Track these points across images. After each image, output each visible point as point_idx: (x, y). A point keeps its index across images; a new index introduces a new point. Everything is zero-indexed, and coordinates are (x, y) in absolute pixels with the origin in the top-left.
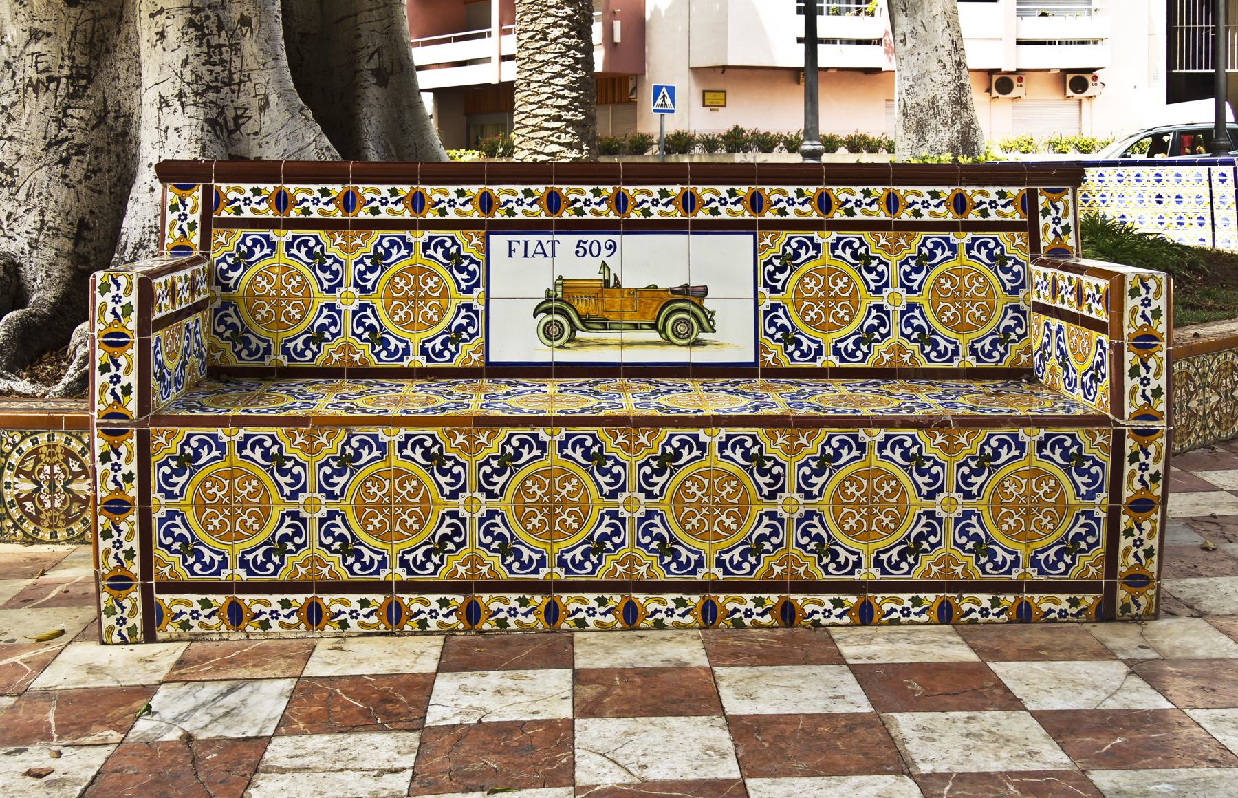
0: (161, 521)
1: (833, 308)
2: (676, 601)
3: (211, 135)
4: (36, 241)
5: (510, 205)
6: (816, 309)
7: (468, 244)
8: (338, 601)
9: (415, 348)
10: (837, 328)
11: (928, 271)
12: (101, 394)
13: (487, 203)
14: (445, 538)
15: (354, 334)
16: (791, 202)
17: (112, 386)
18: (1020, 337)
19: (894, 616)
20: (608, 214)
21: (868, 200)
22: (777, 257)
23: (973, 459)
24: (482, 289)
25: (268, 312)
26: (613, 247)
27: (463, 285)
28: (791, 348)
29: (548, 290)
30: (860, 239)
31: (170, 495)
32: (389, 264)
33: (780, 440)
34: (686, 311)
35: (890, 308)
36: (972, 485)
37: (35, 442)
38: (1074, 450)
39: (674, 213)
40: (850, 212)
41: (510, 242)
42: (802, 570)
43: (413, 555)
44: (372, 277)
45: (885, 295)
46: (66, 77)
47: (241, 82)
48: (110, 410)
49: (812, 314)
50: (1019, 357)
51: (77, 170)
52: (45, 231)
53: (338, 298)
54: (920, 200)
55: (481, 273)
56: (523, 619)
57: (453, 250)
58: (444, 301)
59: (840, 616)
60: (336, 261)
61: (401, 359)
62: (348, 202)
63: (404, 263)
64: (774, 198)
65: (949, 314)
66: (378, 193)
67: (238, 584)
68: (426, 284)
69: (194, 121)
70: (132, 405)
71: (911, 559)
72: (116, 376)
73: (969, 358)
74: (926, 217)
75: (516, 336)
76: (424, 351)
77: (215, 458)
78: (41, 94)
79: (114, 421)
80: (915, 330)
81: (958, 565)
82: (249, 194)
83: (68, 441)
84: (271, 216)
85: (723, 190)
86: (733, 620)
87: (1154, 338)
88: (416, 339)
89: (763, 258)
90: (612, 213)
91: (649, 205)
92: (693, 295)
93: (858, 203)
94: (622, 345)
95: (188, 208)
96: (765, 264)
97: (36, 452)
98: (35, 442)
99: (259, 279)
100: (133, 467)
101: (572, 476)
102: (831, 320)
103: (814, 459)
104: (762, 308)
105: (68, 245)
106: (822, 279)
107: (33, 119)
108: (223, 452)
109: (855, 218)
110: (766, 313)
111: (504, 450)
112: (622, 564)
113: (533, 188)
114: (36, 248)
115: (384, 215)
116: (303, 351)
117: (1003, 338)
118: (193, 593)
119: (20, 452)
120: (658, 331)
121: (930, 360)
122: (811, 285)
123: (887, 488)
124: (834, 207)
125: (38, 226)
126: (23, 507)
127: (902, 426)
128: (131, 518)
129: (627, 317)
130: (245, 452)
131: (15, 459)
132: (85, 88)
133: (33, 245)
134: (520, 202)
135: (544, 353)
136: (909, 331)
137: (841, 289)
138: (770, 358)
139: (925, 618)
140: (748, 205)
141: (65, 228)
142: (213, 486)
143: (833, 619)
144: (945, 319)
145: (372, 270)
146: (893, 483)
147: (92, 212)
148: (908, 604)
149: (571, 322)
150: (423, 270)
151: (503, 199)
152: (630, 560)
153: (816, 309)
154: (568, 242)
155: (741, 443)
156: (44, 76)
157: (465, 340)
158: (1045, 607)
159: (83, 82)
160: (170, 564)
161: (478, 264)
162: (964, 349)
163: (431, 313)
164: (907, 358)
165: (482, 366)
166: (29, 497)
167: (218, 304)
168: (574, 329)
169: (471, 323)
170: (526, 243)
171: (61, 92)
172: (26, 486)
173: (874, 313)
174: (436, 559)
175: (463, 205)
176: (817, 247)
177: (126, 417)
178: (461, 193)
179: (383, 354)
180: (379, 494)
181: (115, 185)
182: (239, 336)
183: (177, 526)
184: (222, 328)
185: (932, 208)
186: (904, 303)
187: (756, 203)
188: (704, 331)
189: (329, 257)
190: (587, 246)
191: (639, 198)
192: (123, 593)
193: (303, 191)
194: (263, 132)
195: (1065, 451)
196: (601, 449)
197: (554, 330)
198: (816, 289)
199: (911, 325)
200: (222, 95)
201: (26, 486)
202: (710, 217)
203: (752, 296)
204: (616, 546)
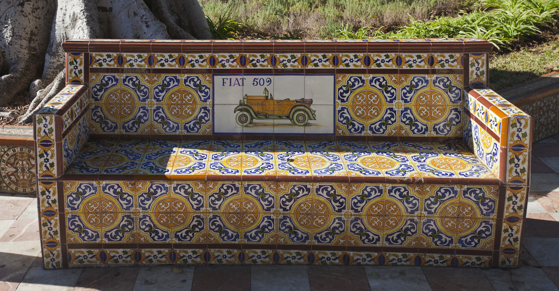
0: (69, 219)
1: (370, 109)
2: (296, 253)
5: (223, 62)
6: (362, 110)
7: (205, 80)
8: (148, 251)
12: (40, 167)
13: (213, 61)
14: (194, 226)
16: (351, 61)
17: (45, 163)
19: (394, 262)
20: (267, 66)
21: (387, 60)
22: (344, 86)
23: (432, 197)
24: (211, 100)
25: (116, 110)
26: (270, 81)
27: (203, 98)
28: (350, 127)
29: (241, 101)
30: (383, 78)
31: (73, 209)
32: (169, 89)
33: (344, 188)
35: (396, 109)
36: (432, 208)
37: (14, 151)
38: (481, 195)
39: (298, 66)
40: (379, 65)
41: (223, 79)
45: (394, 103)
48: (45, 174)
49: (360, 112)
54: (412, 59)
55: (210, 93)
57: (198, 82)
59: (370, 261)
63: (176, 88)
64: (344, 59)
65: (424, 112)
67: (104, 244)
68: (186, 98)
71: (402, 238)
72: (47, 159)
73: (433, 132)
74: (415, 68)
75: (227, 120)
77: (93, 193)
79: (46, 178)
82: (105, 57)
84: (116, 67)
85: (320, 55)
86: (322, 262)
89: (338, 87)
90: (269, 66)
91: (286, 62)
92: (306, 103)
93: (383, 61)
94: (274, 125)
95: (78, 63)
96: (339, 89)
97: (15, 155)
98: (14, 151)
99: (111, 95)
100: (56, 197)
102: (369, 115)
103: (359, 196)
106: (365, 96)
108: (96, 191)
109: (381, 68)
110: (339, 111)
111: (220, 190)
112: (272, 237)
113: (234, 54)
115: (167, 67)
116: (132, 127)
118: (84, 248)
119: (8, 155)
120: (290, 119)
121: (414, 133)
122: (360, 98)
123: (392, 209)
124: (371, 63)
126: (10, 178)
127: (399, 183)
128: (56, 218)
129: (276, 113)
130: (106, 191)
131: (5, 158)
134: (228, 61)
135: (239, 129)
136: (405, 120)
137: (374, 101)
138: (340, 131)
139: (408, 263)
140: (332, 62)
142: (92, 205)
143: (366, 262)
144: (422, 115)
145: (162, 91)
146: (395, 207)
147: (36, 27)
148: (401, 257)
149: (251, 115)
150: (184, 91)
151: (220, 59)
152: (276, 237)
153: (362, 110)
154: (249, 79)
155: (326, 189)
161: (209, 89)
163: (188, 111)
164: (403, 132)
165: (211, 134)
166: (13, 174)
168: (252, 118)
169: (206, 115)
170: (231, 79)
172: (11, 170)
173: (389, 112)
174: (191, 235)
175: (202, 62)
176: (363, 81)
177: (52, 176)
178: (201, 57)
180: (165, 208)
181: (46, 15)
182: (103, 121)
183: (76, 221)
184: (96, 117)
185: (417, 63)
186: (403, 107)
187: (335, 61)
188: (311, 119)
189: (142, 86)
190: (258, 81)
191: (281, 59)
192: (53, 248)
195: (476, 195)
196: (263, 191)
198: (362, 100)
199: (406, 117)
201: (11, 170)
202: (314, 68)
203: (333, 104)
204: (270, 230)
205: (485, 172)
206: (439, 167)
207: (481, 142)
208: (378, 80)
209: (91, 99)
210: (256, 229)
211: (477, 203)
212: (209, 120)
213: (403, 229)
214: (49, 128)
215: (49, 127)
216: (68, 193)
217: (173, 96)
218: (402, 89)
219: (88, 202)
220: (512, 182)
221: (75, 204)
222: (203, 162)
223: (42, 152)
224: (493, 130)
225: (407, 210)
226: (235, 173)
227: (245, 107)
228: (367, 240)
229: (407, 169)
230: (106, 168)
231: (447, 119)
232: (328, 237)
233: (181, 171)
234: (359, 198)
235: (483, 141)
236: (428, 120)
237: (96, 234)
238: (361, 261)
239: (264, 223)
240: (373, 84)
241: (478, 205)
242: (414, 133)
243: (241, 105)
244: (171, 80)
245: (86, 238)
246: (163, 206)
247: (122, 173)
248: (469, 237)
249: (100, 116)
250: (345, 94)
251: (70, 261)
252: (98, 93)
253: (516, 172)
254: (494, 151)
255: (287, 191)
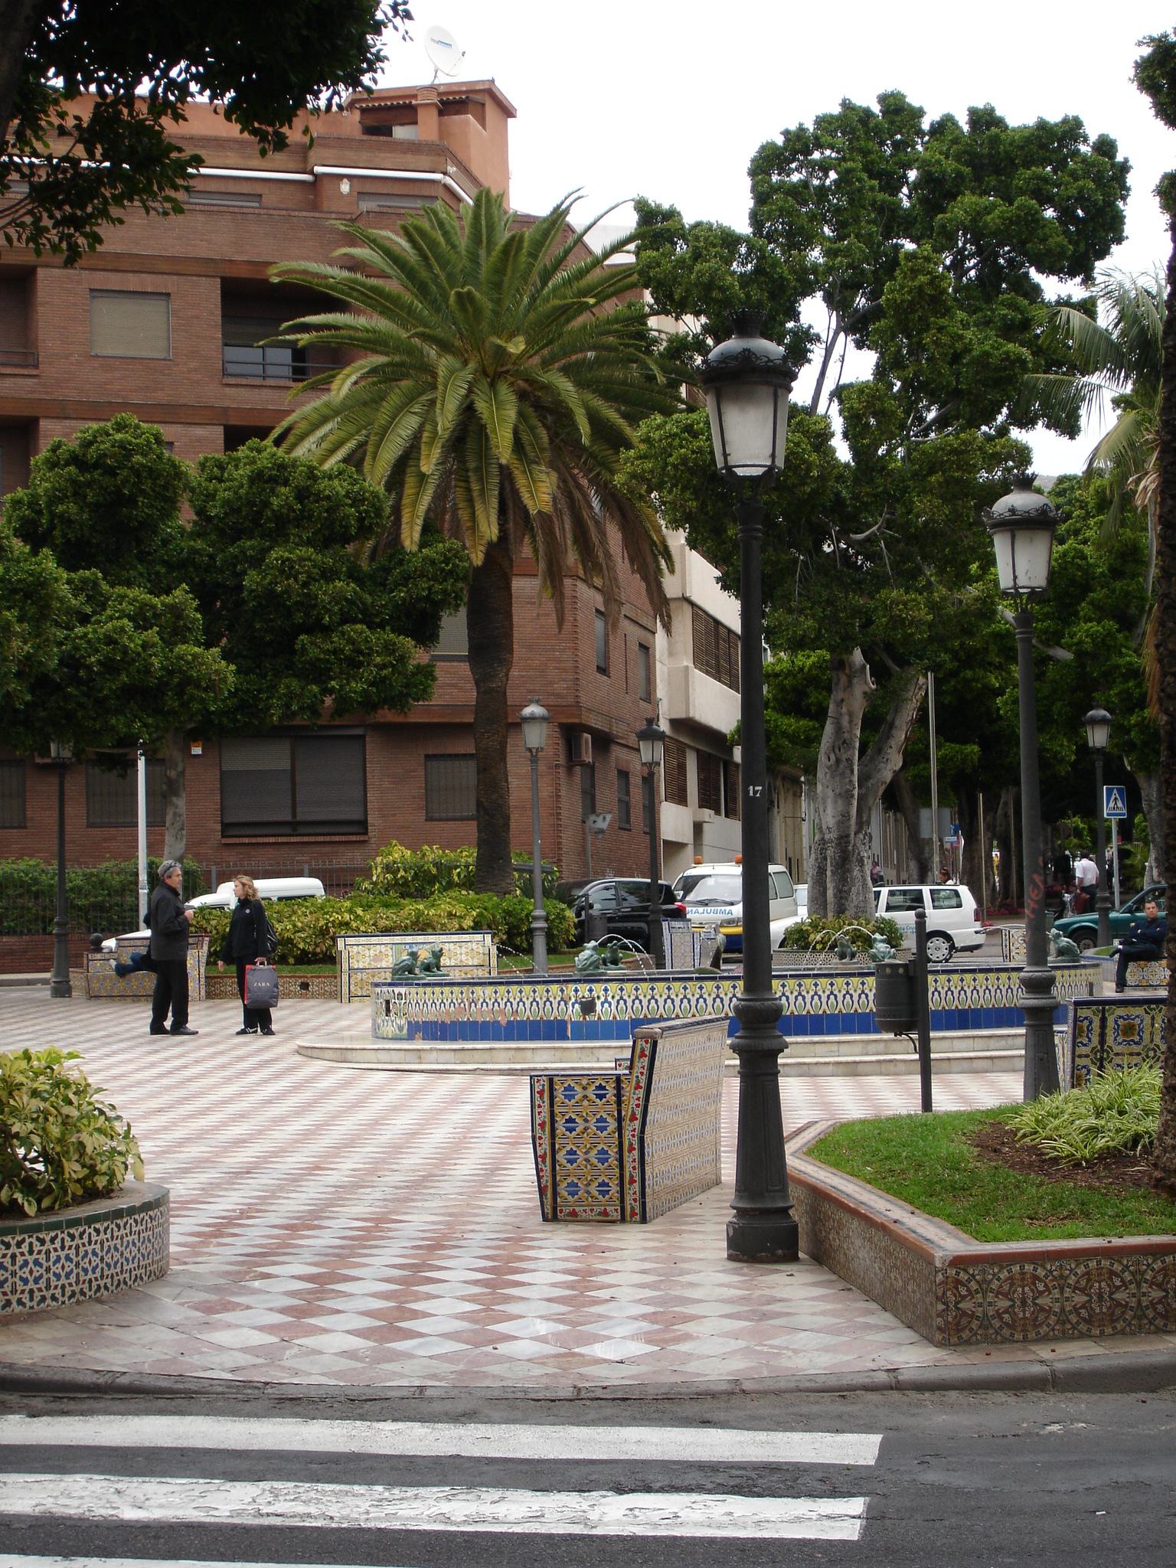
37: (1163, 1262)
83: (1035, 1269)
97: (1011, 1278)
119: (1076, 1274)
126: (1079, 1314)
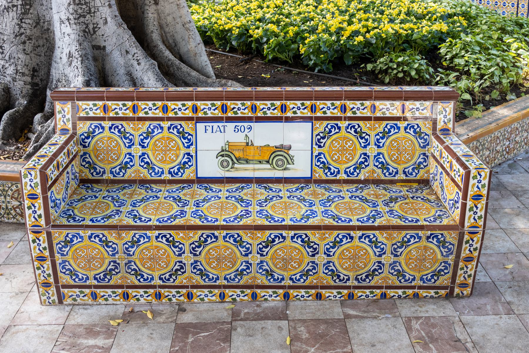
0: (60, 264)
3: (83, 38)
4: (15, 78)
5: (205, 110)
7: (188, 127)
9: (166, 171)
10: (347, 163)
11: (387, 138)
12: (29, 218)
13: (195, 109)
14: (177, 270)
15: (140, 165)
16: (329, 108)
17: (33, 215)
18: (425, 166)
26: (250, 128)
30: (358, 124)
32: (154, 136)
33: (317, 235)
34: (282, 155)
35: (370, 154)
37: (17, 187)
38: (442, 239)
41: (206, 126)
42: (325, 281)
43: (164, 276)
44: (147, 141)
45: (368, 148)
46: (21, 5)
47: (95, 12)
49: (336, 157)
50: (424, 175)
51: (29, 47)
52: (18, 74)
53: (133, 150)
56: (211, 298)
58: (178, 152)
60: (131, 135)
61: (160, 176)
62: (134, 109)
63: (160, 136)
65: (395, 157)
66: (148, 105)
69: (75, 32)
70: (42, 222)
73: (402, 175)
75: (209, 166)
76: (170, 173)
77: (80, 242)
78: (10, 13)
80: (380, 163)
81: (390, 280)
87: (482, 196)
88: (166, 168)
89: (315, 133)
91: (266, 110)
93: (358, 109)
94: (254, 170)
96: (317, 136)
98: (17, 187)
99: (98, 142)
100: (46, 245)
101: (229, 248)
104: (314, 154)
105: (29, 79)
106: (341, 142)
107: (8, 24)
110: (316, 156)
114: (16, 81)
116: (119, 173)
117: (418, 167)
123: (362, 253)
124: (347, 110)
125: (15, 71)
126: (16, 211)
132: (29, 9)
133: (14, 80)
134: (210, 109)
137: (349, 146)
141: (27, 72)
144: (393, 159)
147: (38, 64)
149: (232, 160)
150: (168, 138)
154: (231, 126)
156: (10, 5)
157: (187, 168)
158: (425, 295)
159: (28, 7)
160: (65, 279)
161: (192, 135)
162: (401, 172)
163: (172, 157)
165: (195, 178)
166: (17, 207)
167: (82, 153)
168: (234, 163)
169: (190, 161)
170: (212, 126)
171: (19, 12)
177: (41, 227)
178: (184, 105)
179: (153, 174)
181: (46, 52)
182: (92, 166)
186: (376, 152)
187: (313, 109)
190: (239, 128)
193: (115, 104)
194: (106, 35)
197: (225, 164)
199: (378, 161)
200: (87, 18)
205: (447, 217)
206: (406, 213)
207: (445, 187)
208: (331, 174)
209: (79, 146)
210: (235, 272)
211: (439, 247)
212: (192, 165)
213: (371, 270)
214: (34, 182)
215: (35, 181)
216: (56, 241)
217: (157, 142)
218: (376, 136)
219: (76, 249)
220: (470, 227)
221: (64, 251)
222: (185, 210)
223: (30, 204)
224: (456, 179)
225: (375, 253)
226: (214, 222)
227: (227, 153)
228: (338, 280)
229: (377, 215)
230: (107, 188)
231: (416, 163)
232: (302, 278)
233: (163, 220)
234: (331, 244)
235: (447, 187)
236: (399, 164)
237: (86, 276)
238: (332, 298)
239: (242, 267)
240: (349, 130)
241: (439, 248)
242: (385, 176)
243: (223, 151)
244: (155, 127)
245: (77, 280)
246: (147, 253)
247: (106, 223)
248: (429, 275)
249: (89, 162)
250: (322, 140)
251: (64, 299)
252: (86, 140)
253: (474, 219)
254: (456, 198)
255: (264, 239)
